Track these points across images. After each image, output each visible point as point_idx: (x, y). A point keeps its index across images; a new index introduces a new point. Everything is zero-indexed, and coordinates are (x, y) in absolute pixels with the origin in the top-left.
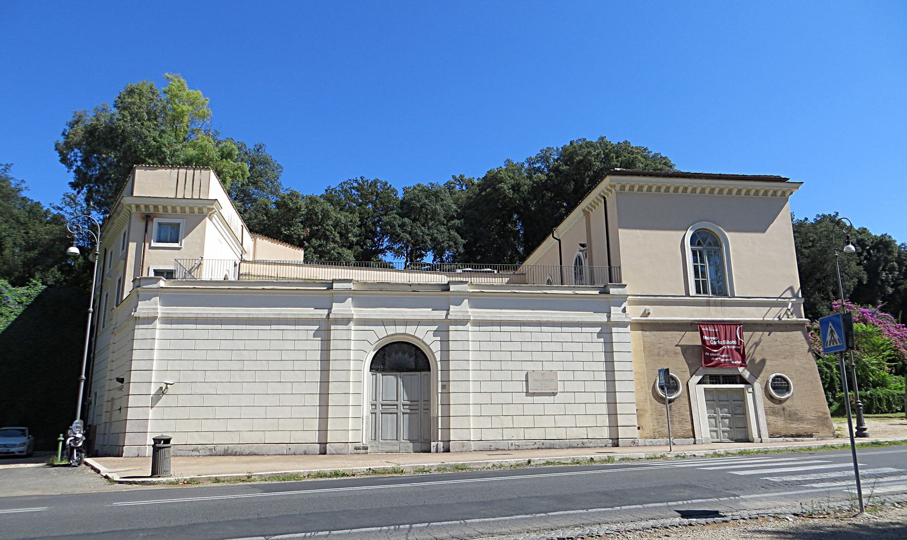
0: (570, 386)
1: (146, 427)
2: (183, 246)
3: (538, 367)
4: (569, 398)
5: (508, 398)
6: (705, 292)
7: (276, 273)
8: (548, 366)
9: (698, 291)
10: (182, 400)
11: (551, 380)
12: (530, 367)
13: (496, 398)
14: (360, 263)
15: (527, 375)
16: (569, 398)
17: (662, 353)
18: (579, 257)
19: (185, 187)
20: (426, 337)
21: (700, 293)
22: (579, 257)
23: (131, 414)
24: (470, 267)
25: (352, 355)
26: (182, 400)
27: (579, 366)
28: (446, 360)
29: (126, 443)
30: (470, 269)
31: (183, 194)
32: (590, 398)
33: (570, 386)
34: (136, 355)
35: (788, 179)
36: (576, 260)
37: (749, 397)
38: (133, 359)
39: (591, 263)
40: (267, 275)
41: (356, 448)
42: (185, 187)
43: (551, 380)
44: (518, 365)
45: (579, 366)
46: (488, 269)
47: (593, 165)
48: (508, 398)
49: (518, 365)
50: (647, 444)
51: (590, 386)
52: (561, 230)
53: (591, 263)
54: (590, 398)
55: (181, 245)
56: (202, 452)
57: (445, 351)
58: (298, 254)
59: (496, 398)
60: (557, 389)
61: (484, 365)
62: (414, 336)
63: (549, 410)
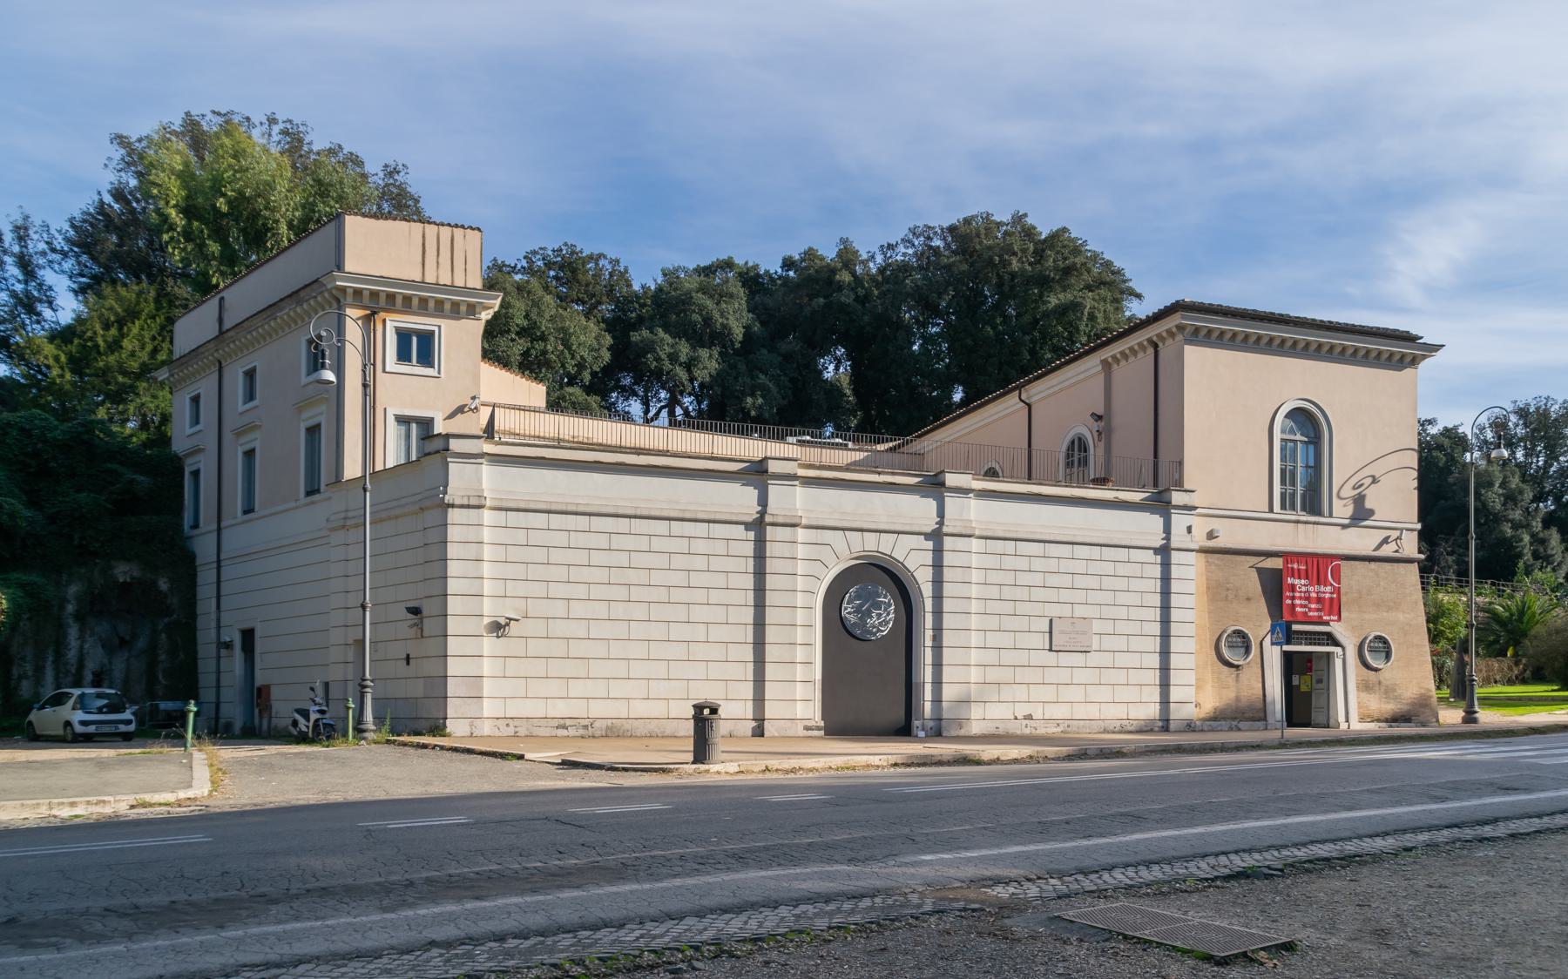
0: (1109, 643)
1: (481, 688)
2: (442, 375)
3: (1065, 611)
4: (1105, 660)
5: (1021, 658)
6: (1293, 508)
7: (557, 431)
8: (1080, 611)
9: (1283, 507)
10: (535, 647)
11: (1084, 633)
12: (1054, 611)
13: (1008, 657)
14: (689, 422)
15: (1051, 621)
16: (1105, 660)
17: (1230, 597)
18: (1080, 439)
19: (438, 263)
20: (915, 559)
21: (1285, 509)
22: (1080, 439)
23: (454, 667)
24: (808, 434)
25: (487, 552)
26: (535, 647)
27: (1122, 612)
28: (938, 597)
29: (450, 713)
30: (808, 438)
31: (435, 274)
32: (1133, 660)
33: (1109, 643)
34: (453, 568)
35: (1421, 338)
36: (1073, 442)
37: (1338, 663)
38: (449, 575)
39: (1108, 450)
40: (527, 433)
41: (807, 728)
42: (438, 263)
43: (1084, 633)
44: (1038, 609)
45: (1122, 612)
46: (837, 440)
47: (574, 262)
48: (1021, 658)
49: (1038, 609)
50: (1206, 728)
51: (1136, 644)
52: (1039, 390)
53: (1108, 450)
54: (1133, 660)
55: (439, 373)
56: (572, 732)
57: (938, 582)
58: (536, 393)
59: (1008, 657)
60: (1091, 647)
61: (515, 555)
62: (890, 556)
63: (1081, 676)
